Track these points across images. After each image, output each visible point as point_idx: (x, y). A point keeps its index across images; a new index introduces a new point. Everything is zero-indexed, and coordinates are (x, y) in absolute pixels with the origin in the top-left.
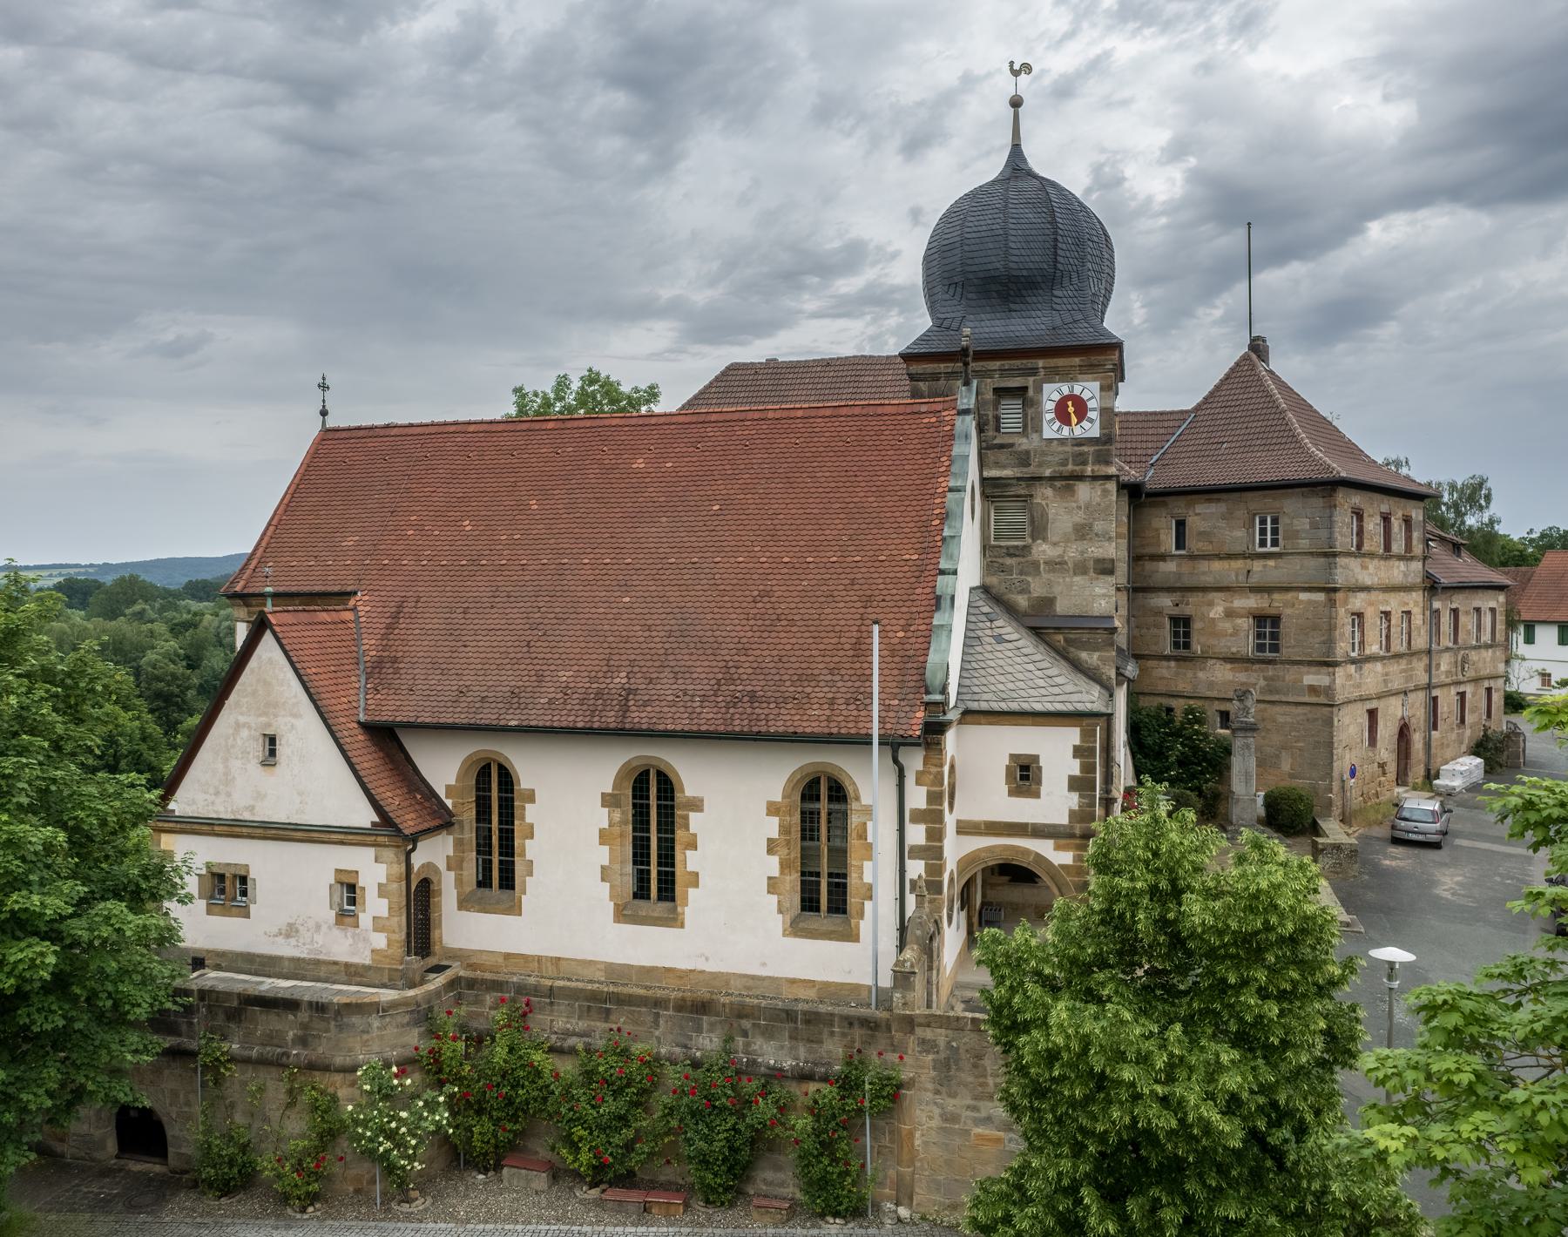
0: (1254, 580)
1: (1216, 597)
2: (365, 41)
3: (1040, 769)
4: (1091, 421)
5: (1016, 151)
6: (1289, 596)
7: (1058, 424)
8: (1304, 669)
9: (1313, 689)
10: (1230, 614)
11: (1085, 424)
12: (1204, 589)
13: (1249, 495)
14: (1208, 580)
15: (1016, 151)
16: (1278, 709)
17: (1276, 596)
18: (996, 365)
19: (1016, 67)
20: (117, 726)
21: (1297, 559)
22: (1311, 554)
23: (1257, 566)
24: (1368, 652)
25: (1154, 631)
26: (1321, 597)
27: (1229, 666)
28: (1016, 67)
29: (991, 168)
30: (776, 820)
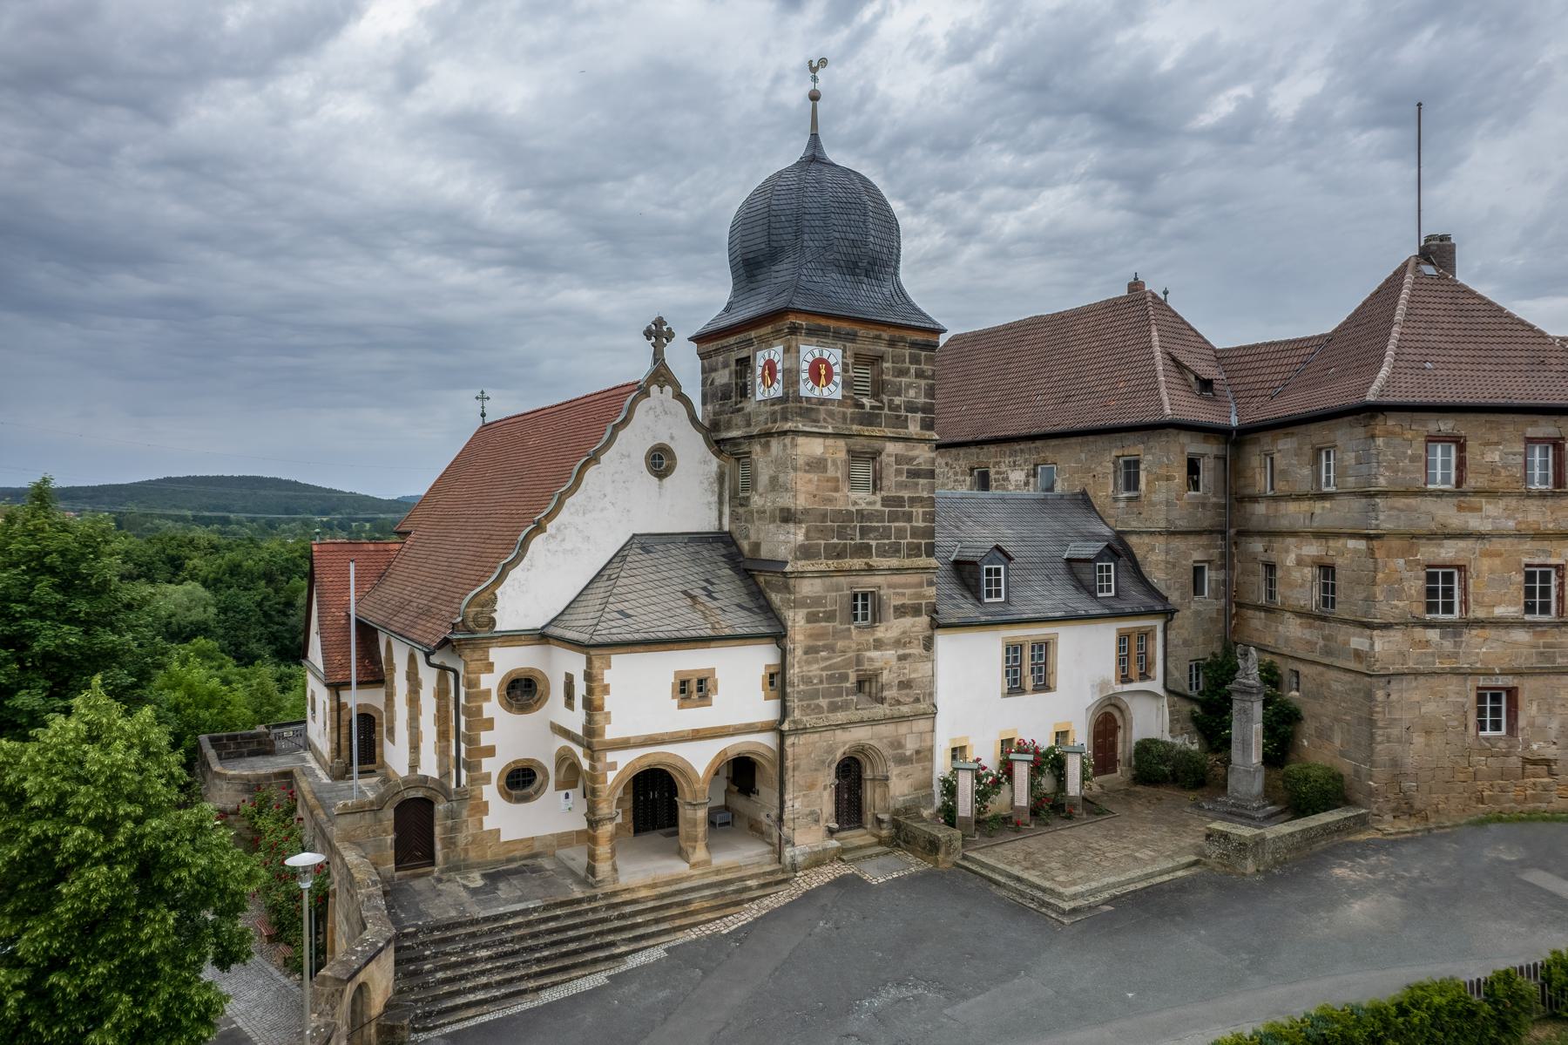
0: (1316, 524)
1: (1291, 541)
2: (270, 87)
3: (716, 682)
4: (836, 385)
5: (815, 140)
6: (1340, 543)
7: (811, 384)
8: (1352, 630)
9: (1358, 655)
10: (1300, 562)
11: (831, 386)
12: (1199, 533)
13: (1312, 427)
14: (1284, 524)
15: (815, 140)
16: (1332, 674)
17: (1331, 543)
18: (732, 340)
19: (815, 64)
20: (1516, 1015)
21: (1344, 501)
22: (1354, 493)
23: (1318, 507)
24: (1471, 615)
25: (1252, 578)
26: (1361, 545)
27: (1299, 621)
28: (815, 64)
29: (791, 153)
30: (486, 715)
